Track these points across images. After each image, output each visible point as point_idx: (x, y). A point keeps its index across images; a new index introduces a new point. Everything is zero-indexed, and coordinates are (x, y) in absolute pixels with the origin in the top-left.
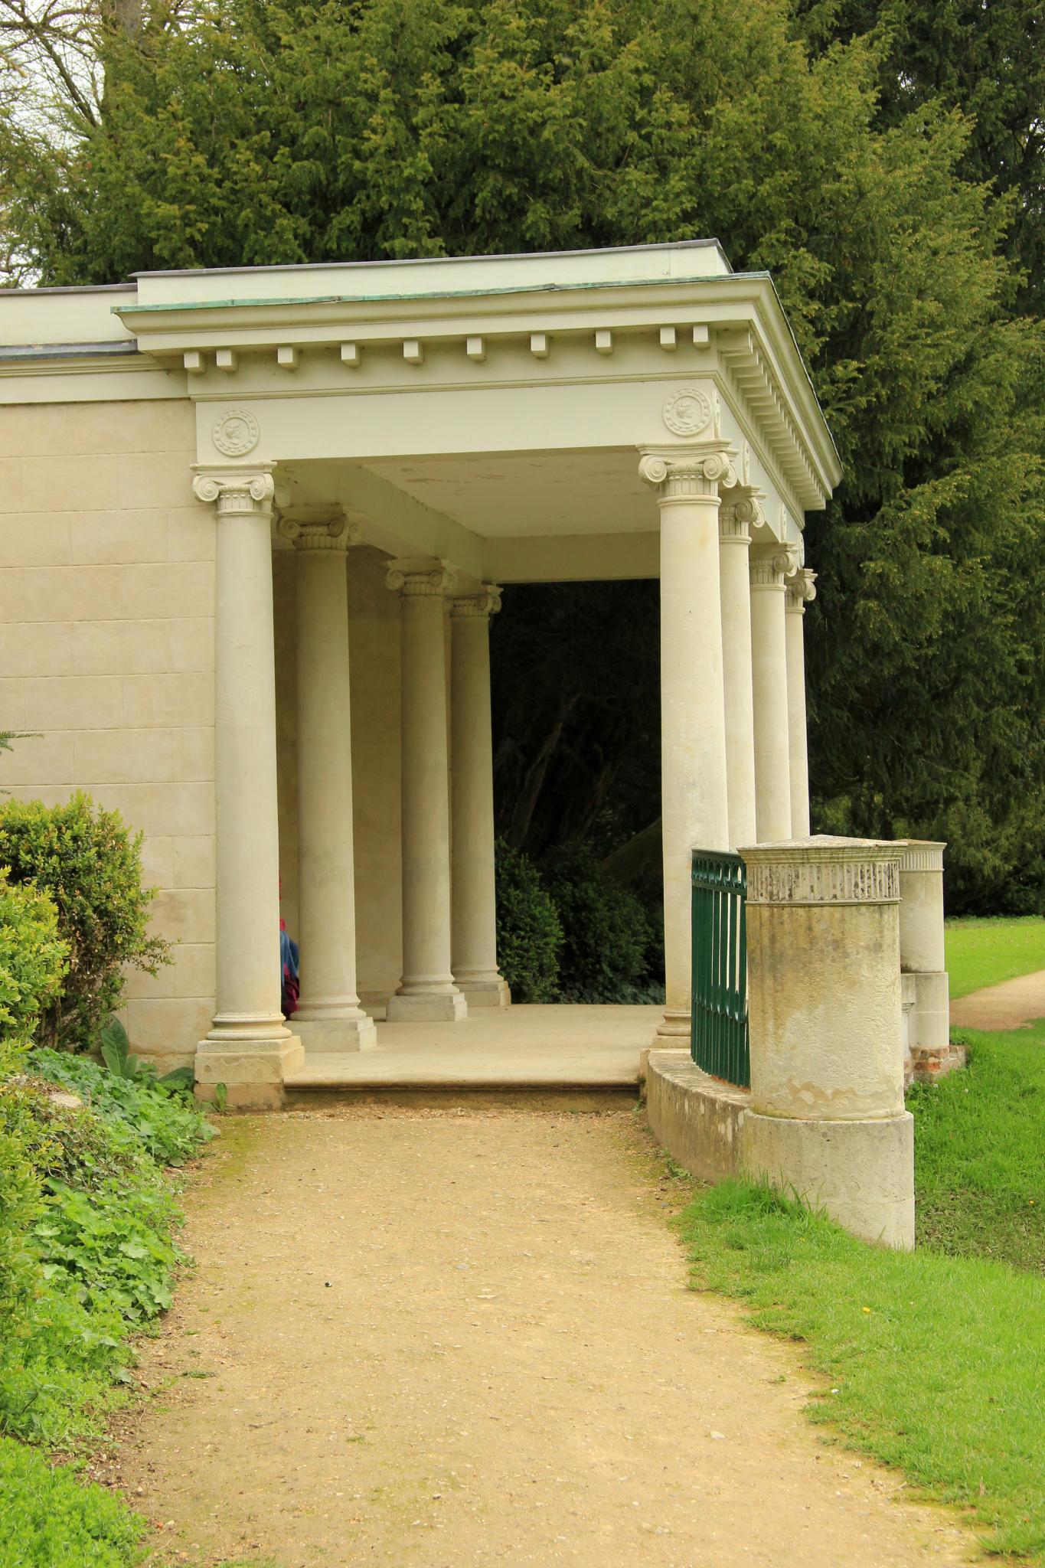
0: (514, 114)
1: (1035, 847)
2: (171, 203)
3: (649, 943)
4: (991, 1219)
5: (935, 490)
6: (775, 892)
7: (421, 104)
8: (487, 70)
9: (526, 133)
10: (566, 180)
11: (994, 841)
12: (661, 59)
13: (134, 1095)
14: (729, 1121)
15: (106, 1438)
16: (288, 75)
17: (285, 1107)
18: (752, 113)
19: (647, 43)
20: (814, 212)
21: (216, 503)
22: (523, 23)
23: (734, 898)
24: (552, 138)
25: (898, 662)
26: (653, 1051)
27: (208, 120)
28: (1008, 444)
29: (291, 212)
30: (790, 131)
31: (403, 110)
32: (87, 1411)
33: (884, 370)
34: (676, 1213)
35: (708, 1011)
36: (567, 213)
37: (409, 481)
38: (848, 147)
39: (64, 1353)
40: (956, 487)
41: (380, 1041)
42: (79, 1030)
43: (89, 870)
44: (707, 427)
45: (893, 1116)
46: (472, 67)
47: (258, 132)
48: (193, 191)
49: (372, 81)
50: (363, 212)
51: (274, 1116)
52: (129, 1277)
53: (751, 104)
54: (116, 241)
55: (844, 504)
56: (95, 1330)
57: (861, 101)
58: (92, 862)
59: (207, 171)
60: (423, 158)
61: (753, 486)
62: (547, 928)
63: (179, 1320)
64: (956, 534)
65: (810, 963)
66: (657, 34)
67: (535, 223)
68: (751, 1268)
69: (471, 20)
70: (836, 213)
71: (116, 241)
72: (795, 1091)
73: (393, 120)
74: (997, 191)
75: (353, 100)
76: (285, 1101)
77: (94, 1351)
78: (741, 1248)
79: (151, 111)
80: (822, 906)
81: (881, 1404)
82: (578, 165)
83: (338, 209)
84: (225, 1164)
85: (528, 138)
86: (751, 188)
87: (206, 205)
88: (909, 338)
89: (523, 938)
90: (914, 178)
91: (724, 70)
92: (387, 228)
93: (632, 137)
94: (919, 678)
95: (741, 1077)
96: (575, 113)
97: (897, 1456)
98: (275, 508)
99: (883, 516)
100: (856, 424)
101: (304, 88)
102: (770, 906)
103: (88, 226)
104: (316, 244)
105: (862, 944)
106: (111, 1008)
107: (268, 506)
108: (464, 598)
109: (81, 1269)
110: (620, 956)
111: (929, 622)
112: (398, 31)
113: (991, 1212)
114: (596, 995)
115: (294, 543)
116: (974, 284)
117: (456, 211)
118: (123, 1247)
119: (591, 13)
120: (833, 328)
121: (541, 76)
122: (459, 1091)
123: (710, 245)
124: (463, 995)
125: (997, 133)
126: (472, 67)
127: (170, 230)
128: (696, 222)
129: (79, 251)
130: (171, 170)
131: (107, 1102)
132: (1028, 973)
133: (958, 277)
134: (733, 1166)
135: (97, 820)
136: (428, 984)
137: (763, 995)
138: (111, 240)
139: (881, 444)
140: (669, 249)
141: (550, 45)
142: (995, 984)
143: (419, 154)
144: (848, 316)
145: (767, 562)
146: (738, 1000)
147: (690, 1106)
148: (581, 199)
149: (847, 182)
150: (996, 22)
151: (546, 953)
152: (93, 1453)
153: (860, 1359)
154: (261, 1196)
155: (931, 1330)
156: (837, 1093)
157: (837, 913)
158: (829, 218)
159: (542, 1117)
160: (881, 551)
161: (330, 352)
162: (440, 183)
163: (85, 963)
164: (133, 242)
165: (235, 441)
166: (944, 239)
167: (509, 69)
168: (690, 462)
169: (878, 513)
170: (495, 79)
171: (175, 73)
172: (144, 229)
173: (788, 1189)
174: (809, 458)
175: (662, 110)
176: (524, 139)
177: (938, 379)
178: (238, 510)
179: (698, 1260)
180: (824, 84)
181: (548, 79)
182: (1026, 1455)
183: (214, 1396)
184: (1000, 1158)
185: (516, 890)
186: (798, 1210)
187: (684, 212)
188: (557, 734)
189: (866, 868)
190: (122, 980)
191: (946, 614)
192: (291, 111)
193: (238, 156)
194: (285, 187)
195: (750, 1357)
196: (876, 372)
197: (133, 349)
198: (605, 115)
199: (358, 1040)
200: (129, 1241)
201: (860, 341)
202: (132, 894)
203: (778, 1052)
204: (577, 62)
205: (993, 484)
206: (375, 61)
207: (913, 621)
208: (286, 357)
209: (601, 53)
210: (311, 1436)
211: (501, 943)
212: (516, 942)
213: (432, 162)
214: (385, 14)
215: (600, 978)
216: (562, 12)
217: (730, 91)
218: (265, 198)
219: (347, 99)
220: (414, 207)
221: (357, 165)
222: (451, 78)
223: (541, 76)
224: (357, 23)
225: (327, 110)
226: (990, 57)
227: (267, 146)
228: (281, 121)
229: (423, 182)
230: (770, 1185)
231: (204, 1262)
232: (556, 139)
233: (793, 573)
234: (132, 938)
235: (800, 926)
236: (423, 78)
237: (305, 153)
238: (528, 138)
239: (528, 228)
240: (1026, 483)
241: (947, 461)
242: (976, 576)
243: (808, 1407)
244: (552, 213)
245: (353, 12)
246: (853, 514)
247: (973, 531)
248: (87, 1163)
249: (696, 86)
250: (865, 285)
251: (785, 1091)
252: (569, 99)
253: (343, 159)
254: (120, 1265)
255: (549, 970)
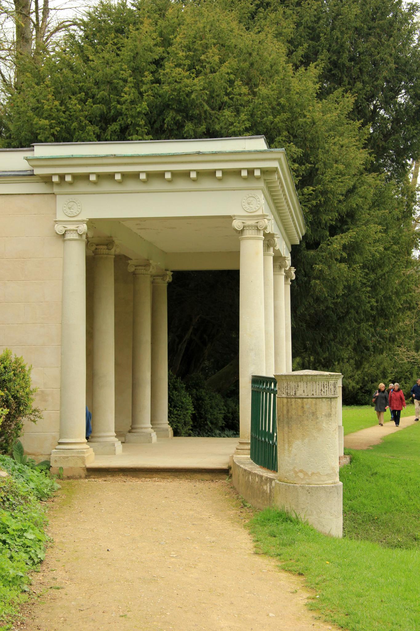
0: (180, 88)
1: (368, 379)
2: (46, 120)
3: (225, 413)
4: (360, 524)
5: (342, 237)
6: (289, 392)
7: (144, 84)
8: (170, 71)
9: (185, 96)
10: (200, 115)
11: (353, 376)
12: (237, 69)
13: (27, 471)
14: (268, 484)
15: (19, 615)
16: (92, 71)
17: (87, 477)
18: (272, 91)
19: (231, 63)
20: (296, 129)
21: (64, 235)
22: (184, 54)
23: (266, 394)
24: (195, 98)
25: (326, 304)
26: (235, 456)
27: (60, 88)
28: (368, 221)
29: (92, 124)
30: (287, 98)
31: (137, 86)
32: (11, 603)
33: (322, 191)
34: (247, 522)
35: (259, 440)
36: (200, 127)
37: (138, 229)
38: (308, 105)
39: (2, 579)
40: (350, 237)
41: (123, 451)
42: (4, 445)
43: (10, 380)
44: (259, 209)
45: (335, 483)
46: (164, 70)
47: (80, 93)
48: (54, 115)
49: (126, 74)
50: (121, 125)
51: (82, 480)
52: (27, 547)
53: (272, 87)
54: (23, 134)
55: (306, 242)
56: (14, 569)
57: (312, 87)
58: (11, 377)
59: (59, 107)
60: (144, 104)
61: (275, 233)
62: (188, 407)
63: (48, 565)
64: (349, 255)
65: (303, 421)
66: (236, 60)
67: (188, 131)
68: (279, 545)
69: (163, 52)
70: (304, 130)
71: (23, 134)
72: (296, 473)
73: (133, 89)
74: (364, 125)
75: (118, 81)
76: (87, 474)
77: (14, 578)
78: (275, 537)
79: (37, 84)
80: (308, 398)
81: (338, 602)
82: (205, 109)
83: (111, 123)
84: (64, 500)
85: (186, 98)
86: (272, 120)
87: (59, 121)
88: (332, 179)
89: (178, 411)
90: (333, 118)
91: (261, 75)
92: (130, 131)
93: (226, 98)
94: (333, 311)
95: (272, 466)
96: (204, 89)
97: (346, 624)
98: (87, 238)
99: (321, 247)
100: (311, 211)
101: (98, 77)
102: (287, 398)
103: (11, 127)
104: (102, 137)
105: (323, 414)
106: (18, 436)
107: (84, 236)
108: (158, 276)
109: (8, 543)
110: (214, 418)
111: (339, 289)
112: (135, 56)
113: (360, 521)
114: (204, 434)
115: (93, 252)
116: (357, 159)
117: (157, 125)
118: (25, 534)
119: (211, 51)
120: (303, 174)
121: (191, 74)
122: (157, 471)
123: (261, 138)
124: (155, 433)
125: (363, 103)
126: (164, 70)
127: (45, 130)
128: (250, 132)
129: (7, 138)
130: (46, 107)
131: (17, 474)
132: (368, 428)
133: (351, 156)
134: (270, 503)
135: (13, 360)
136: (142, 428)
137: (283, 434)
138: (21, 134)
139: (320, 219)
140: (245, 139)
141: (194, 63)
142: (356, 432)
143: (143, 103)
144: (309, 169)
145: (278, 264)
146: (271, 436)
147: (252, 478)
148: (206, 122)
149: (308, 118)
150: (362, 61)
151: (187, 417)
152: (14, 622)
153: (327, 583)
154: (79, 513)
155: (354, 571)
156: (313, 474)
157: (314, 401)
158: (301, 132)
159: (190, 482)
160: (321, 261)
161: (111, 176)
162: (151, 115)
163: (8, 418)
164: (30, 134)
165: (72, 211)
166: (345, 141)
167: (179, 71)
168: (252, 222)
169: (320, 246)
170: (173, 75)
171: (48, 69)
172: (34, 130)
173: (293, 512)
174: (294, 224)
175: (238, 88)
176: (184, 98)
177: (343, 195)
178: (72, 238)
179: (257, 541)
180: (300, 81)
181: (194, 75)
182: (398, 625)
183: (63, 597)
184: (363, 500)
185: (176, 391)
186: (297, 521)
187: (246, 128)
188: (191, 331)
189: (325, 383)
190: (22, 425)
191: (345, 287)
192: (93, 85)
193: (72, 102)
194: (90, 115)
195: (282, 582)
196: (319, 192)
197: (32, 173)
198: (216, 90)
199: (115, 450)
200: (28, 532)
201: (313, 180)
202: (27, 390)
203: (289, 457)
204: (205, 69)
205: (363, 236)
206: (126, 66)
207: (332, 288)
208: (93, 178)
209: (214, 66)
210: (105, 614)
211: (170, 412)
212: (176, 412)
213: (148, 106)
214: (130, 49)
215: (206, 427)
216: (199, 50)
217: (263, 82)
218: (82, 119)
219: (115, 81)
220: (141, 123)
221: (119, 106)
222: (156, 74)
223: (191, 74)
224: (119, 52)
225: (107, 85)
226: (360, 74)
227: (83, 99)
228: (89, 89)
229: (144, 114)
230: (286, 511)
231: (57, 540)
232: (197, 98)
233: (287, 269)
234: (27, 408)
235: (299, 406)
236: (145, 74)
237: (98, 101)
238: (186, 98)
239: (185, 133)
240: (376, 236)
241: (346, 227)
242: (356, 271)
243: (308, 603)
244: (194, 127)
245: (118, 48)
246: (310, 246)
247: (355, 254)
248: (10, 499)
249: (250, 80)
250: (315, 158)
251: (292, 473)
252: (202, 83)
253: (113, 104)
254: (24, 542)
255: (188, 424)
